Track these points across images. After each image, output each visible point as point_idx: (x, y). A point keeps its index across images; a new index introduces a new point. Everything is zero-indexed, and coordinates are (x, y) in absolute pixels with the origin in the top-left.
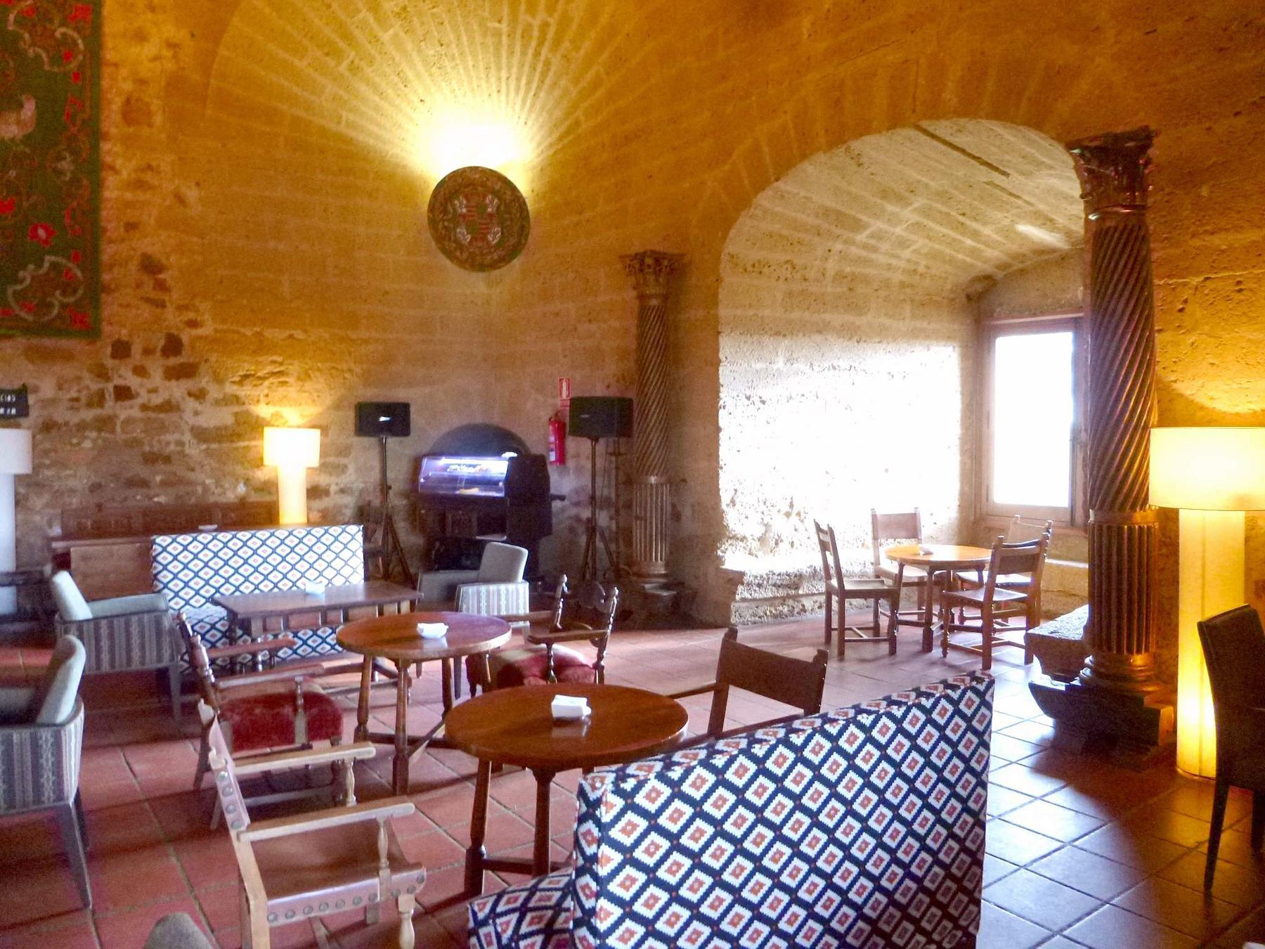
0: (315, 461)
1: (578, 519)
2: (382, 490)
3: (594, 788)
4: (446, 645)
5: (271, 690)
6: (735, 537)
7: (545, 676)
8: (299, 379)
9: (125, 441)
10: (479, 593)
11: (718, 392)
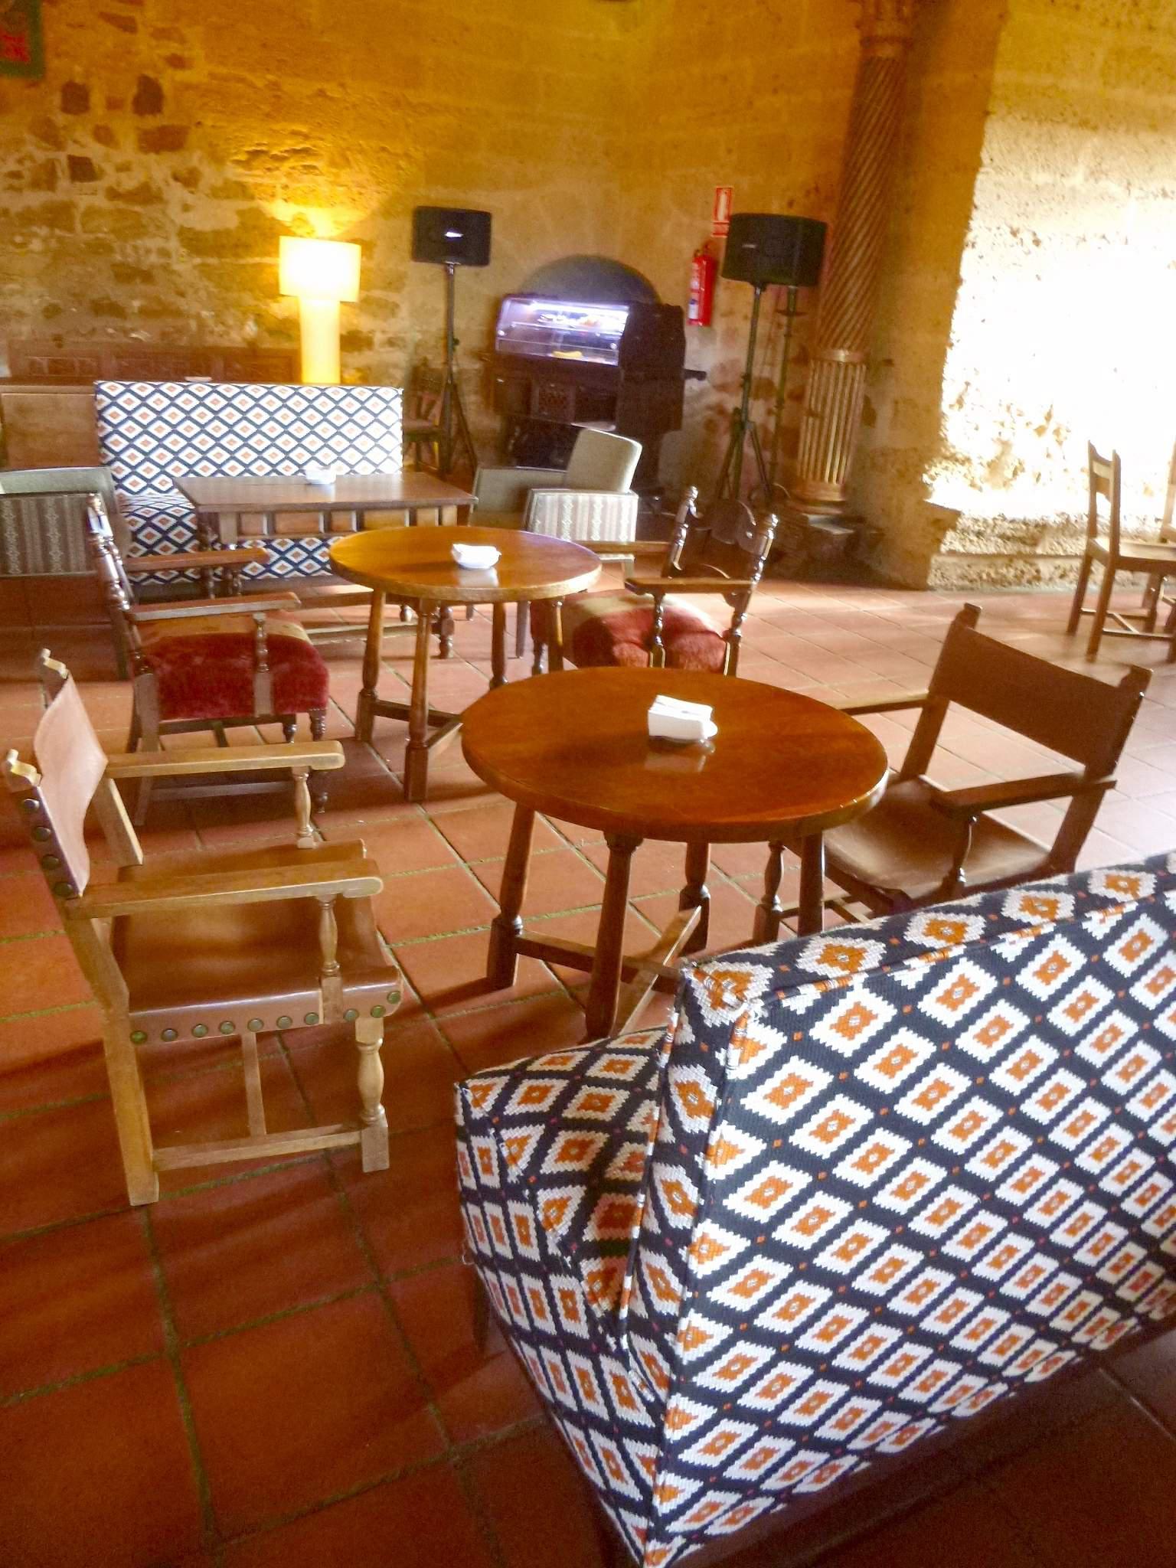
0: (352, 294)
1: (720, 410)
2: (446, 346)
3: (718, 1003)
4: (496, 582)
5: (224, 629)
6: (953, 458)
7: (648, 644)
8: (333, 164)
9: (88, 244)
10: (592, 504)
11: (968, 217)
